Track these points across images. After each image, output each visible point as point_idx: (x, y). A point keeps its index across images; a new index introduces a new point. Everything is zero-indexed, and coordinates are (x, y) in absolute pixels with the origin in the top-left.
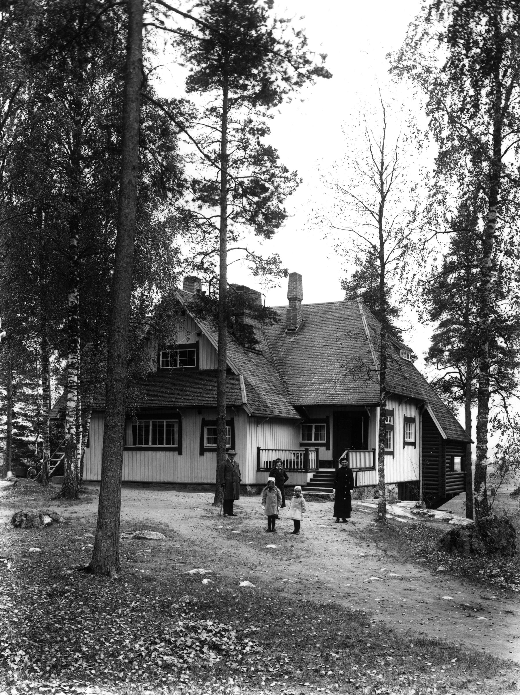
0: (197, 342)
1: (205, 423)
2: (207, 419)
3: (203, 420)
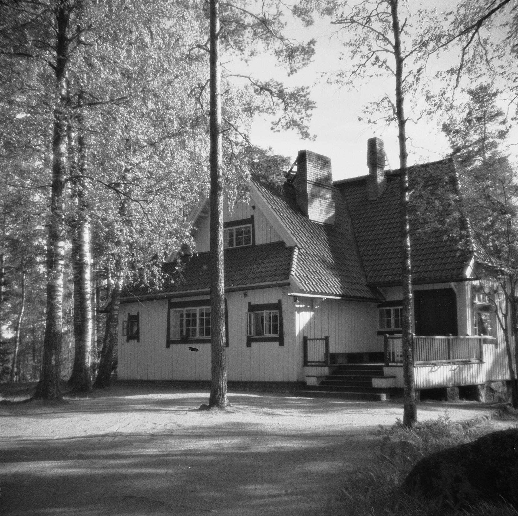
0: (253, 216)
1: (252, 308)
2: (253, 303)
3: (250, 303)
